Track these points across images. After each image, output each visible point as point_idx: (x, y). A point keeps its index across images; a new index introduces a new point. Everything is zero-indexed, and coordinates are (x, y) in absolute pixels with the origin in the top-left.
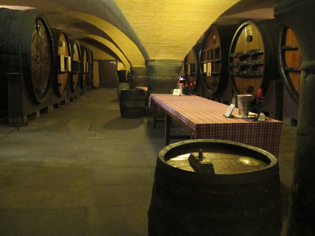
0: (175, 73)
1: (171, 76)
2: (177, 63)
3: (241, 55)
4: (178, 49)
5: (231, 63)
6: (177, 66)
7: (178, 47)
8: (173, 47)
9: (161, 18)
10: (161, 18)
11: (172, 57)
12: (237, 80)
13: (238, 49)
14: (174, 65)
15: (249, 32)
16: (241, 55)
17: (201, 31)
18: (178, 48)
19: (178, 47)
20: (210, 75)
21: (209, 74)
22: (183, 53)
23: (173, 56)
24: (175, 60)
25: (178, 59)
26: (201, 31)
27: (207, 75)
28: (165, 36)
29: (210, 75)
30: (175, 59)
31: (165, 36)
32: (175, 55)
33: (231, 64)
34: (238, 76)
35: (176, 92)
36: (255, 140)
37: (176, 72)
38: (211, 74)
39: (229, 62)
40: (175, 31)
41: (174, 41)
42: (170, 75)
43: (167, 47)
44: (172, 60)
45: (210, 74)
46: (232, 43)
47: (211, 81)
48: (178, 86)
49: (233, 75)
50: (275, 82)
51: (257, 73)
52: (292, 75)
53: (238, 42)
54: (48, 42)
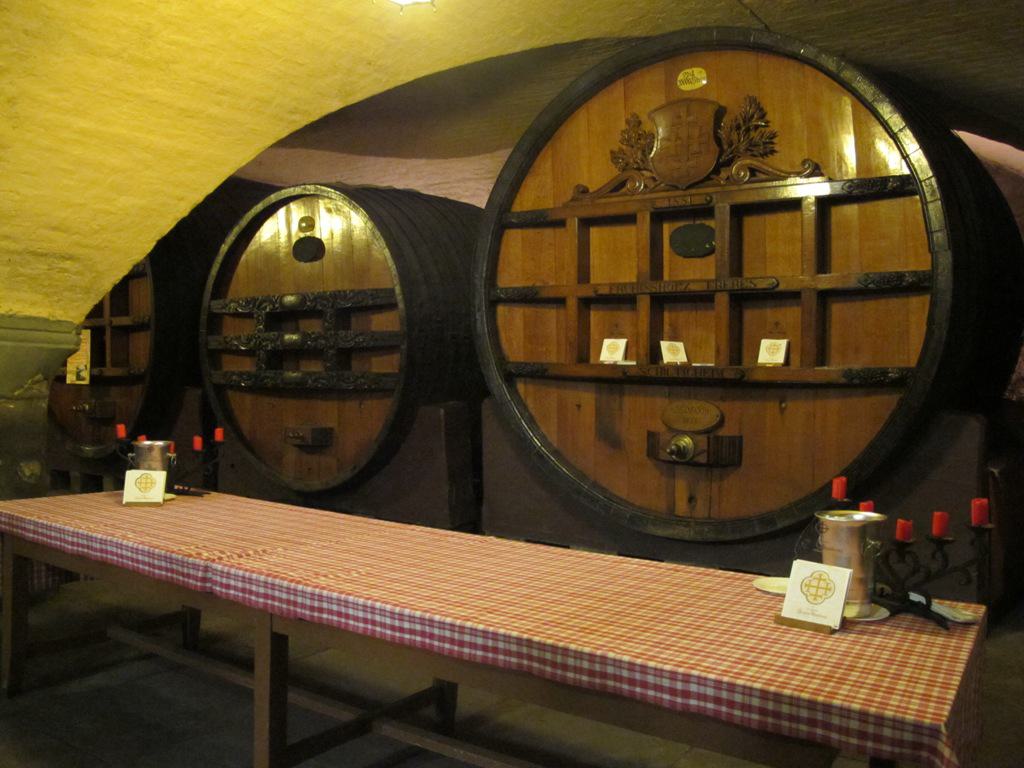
0: (38, 382)
1: (17, 399)
2: (54, 336)
3: (274, 308)
4: (65, 270)
5: (210, 338)
6: (57, 349)
7: (70, 258)
8: (42, 255)
9: (12, 101)
10: (12, 101)
11: (33, 304)
12: (244, 406)
13: (242, 286)
14: (45, 345)
15: (304, 225)
16: (274, 308)
17: (182, 199)
18: (68, 264)
19: (70, 258)
20: (86, 382)
21: (79, 377)
22: (87, 291)
23: (38, 297)
24: (46, 320)
25: (59, 314)
26: (182, 199)
27: (68, 382)
28: (17, 197)
29: (86, 382)
30: (42, 312)
31: (17, 197)
32: (47, 295)
33: (214, 343)
34: (258, 388)
35: (144, 485)
36: (542, 653)
37: (45, 379)
38: (92, 377)
39: (203, 330)
40: (72, 183)
41: (54, 229)
42: (16, 393)
43: (13, 252)
44: (35, 318)
45: (86, 374)
46: (220, 259)
47: (87, 407)
48: (138, 455)
49: (223, 381)
50: (442, 411)
51: (234, 377)
52: (531, 388)
53: (244, 257)
54: (839, 126)
